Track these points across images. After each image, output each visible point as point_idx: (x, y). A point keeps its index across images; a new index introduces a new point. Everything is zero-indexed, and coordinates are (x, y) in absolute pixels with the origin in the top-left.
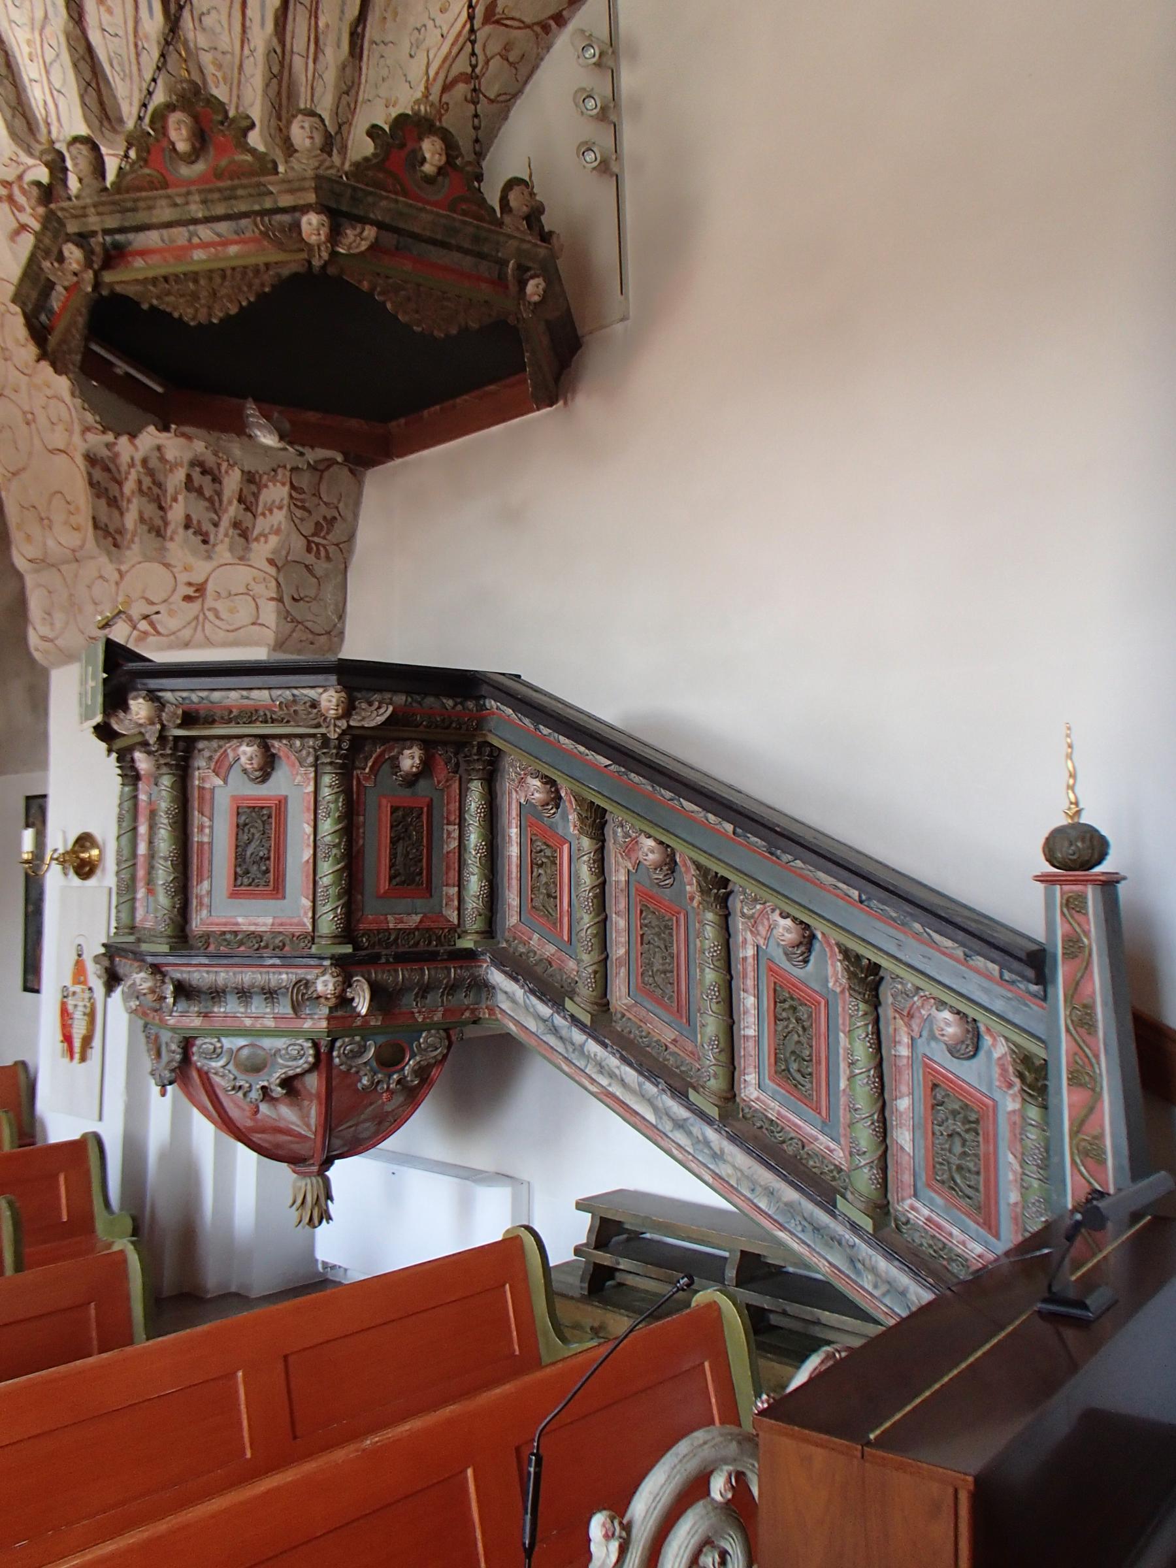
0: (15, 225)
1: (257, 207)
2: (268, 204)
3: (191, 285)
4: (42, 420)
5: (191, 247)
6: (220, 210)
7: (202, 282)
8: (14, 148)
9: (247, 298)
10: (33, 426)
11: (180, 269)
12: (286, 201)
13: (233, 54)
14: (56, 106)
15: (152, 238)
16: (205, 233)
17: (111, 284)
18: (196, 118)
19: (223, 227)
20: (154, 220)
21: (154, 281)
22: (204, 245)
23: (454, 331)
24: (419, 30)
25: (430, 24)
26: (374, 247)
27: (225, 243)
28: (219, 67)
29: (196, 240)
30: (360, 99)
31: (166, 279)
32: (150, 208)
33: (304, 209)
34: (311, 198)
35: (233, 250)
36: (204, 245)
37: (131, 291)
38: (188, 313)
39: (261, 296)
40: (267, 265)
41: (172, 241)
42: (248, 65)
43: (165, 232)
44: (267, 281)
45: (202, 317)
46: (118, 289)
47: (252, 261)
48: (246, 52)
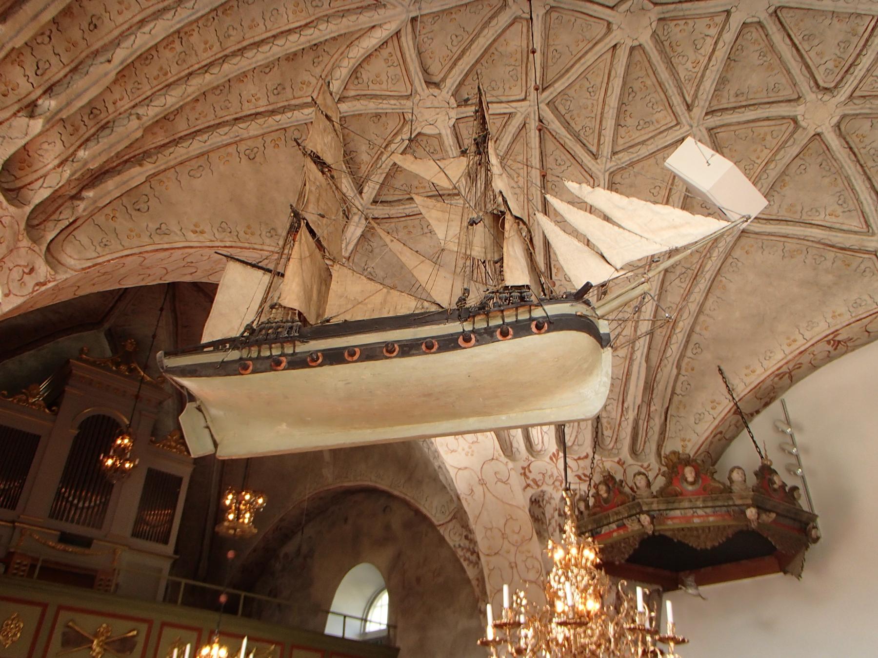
0: (525, 484)
1: (726, 504)
2: (731, 503)
3: (695, 532)
4: (521, 566)
5: (693, 516)
6: (710, 504)
7: (700, 531)
8: (528, 454)
9: (722, 540)
10: (515, 570)
11: (688, 526)
12: (739, 502)
13: (616, 419)
14: (543, 438)
15: (677, 513)
16: (700, 512)
17: (659, 531)
18: (693, 466)
19: (708, 510)
20: (681, 507)
21: (678, 530)
22: (699, 516)
23: (724, 539)
24: (700, 415)
25: (706, 413)
26: (774, 521)
27: (708, 516)
28: (609, 423)
29: (696, 514)
30: (667, 436)
31: (683, 529)
32: (680, 502)
33: (748, 506)
34: (750, 502)
35: (711, 519)
36: (699, 516)
37: (669, 534)
38: (693, 543)
39: (728, 539)
40: (729, 526)
41: (685, 514)
42: (624, 424)
43: (683, 511)
44: (730, 532)
45: (703, 546)
46: (662, 533)
47: (721, 524)
48: (623, 419)
